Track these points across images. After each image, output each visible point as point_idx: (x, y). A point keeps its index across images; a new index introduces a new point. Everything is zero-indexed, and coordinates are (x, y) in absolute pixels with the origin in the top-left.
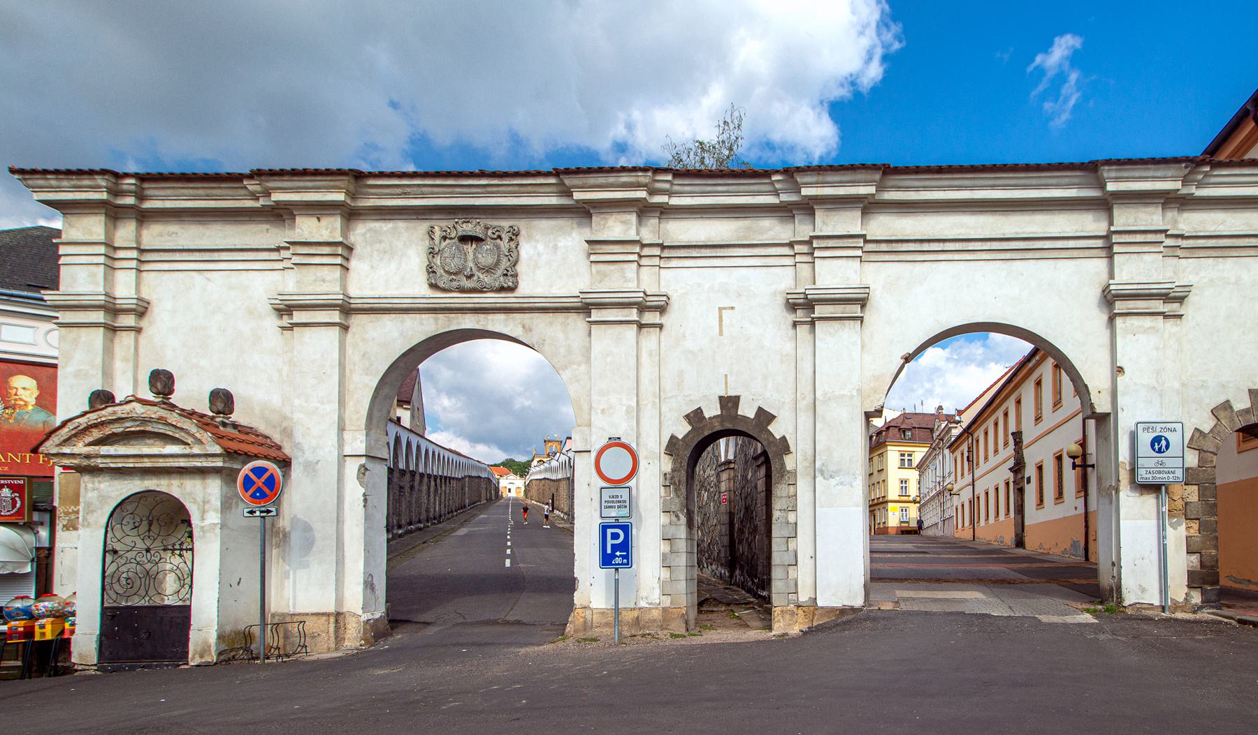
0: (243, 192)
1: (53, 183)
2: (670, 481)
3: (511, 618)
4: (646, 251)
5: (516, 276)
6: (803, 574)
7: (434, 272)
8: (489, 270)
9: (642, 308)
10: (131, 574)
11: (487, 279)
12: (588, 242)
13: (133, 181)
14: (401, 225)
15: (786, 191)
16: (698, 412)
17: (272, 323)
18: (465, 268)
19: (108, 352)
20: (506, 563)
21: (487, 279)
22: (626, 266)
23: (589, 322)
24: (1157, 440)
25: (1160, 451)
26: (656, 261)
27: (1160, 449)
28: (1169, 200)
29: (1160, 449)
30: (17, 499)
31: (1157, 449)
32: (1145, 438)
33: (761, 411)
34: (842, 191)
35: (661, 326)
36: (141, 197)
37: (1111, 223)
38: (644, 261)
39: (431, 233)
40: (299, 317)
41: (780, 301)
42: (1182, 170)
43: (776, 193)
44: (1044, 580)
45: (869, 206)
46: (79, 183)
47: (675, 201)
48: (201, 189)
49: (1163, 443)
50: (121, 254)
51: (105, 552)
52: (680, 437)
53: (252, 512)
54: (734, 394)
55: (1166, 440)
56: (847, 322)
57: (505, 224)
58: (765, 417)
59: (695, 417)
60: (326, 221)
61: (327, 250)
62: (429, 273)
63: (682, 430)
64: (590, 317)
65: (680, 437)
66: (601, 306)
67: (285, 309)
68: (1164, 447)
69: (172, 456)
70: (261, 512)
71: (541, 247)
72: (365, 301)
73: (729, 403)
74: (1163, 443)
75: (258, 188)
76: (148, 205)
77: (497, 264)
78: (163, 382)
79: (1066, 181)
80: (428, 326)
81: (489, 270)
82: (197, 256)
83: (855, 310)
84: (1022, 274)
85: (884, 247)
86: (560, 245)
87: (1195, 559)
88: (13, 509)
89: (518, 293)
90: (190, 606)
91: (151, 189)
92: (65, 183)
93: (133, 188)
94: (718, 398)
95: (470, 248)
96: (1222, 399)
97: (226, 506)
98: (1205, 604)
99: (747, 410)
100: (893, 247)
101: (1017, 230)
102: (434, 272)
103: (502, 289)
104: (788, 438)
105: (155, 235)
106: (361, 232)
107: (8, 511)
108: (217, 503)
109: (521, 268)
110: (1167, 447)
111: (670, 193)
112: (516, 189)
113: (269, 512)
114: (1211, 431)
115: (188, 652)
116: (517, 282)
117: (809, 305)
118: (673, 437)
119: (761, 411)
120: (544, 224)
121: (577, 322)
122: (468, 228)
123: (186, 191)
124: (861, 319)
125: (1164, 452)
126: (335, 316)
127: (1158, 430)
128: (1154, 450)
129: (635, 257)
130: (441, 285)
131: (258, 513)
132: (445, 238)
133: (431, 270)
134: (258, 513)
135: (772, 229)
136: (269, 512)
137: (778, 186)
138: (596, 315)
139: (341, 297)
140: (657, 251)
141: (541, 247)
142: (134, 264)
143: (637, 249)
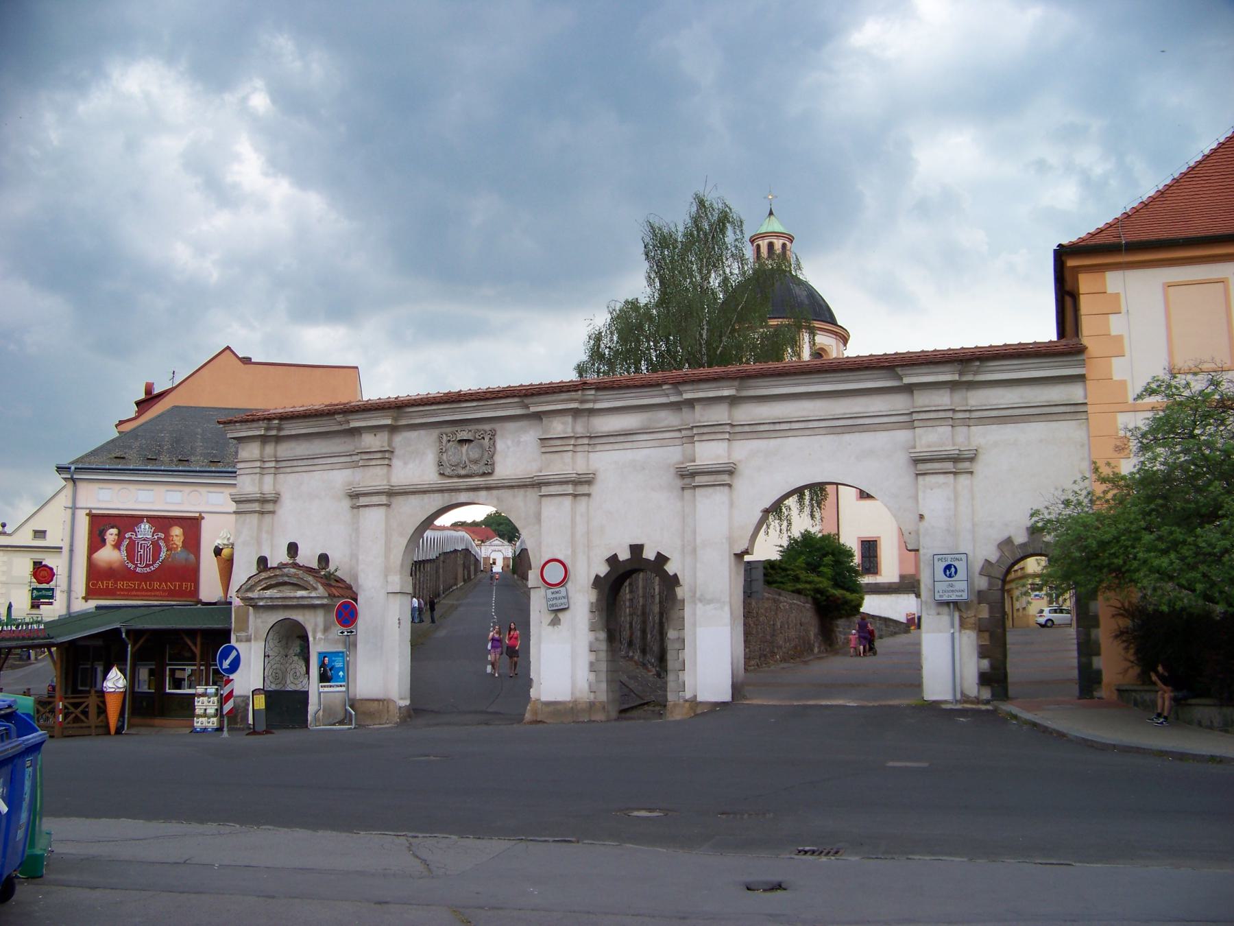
0: (334, 421)
1: (238, 427)
2: (596, 608)
3: (490, 710)
4: (580, 441)
5: (493, 464)
6: (687, 677)
7: (442, 465)
8: (476, 462)
9: (576, 483)
10: (278, 671)
11: (475, 468)
12: (540, 439)
13: (277, 422)
14: (422, 432)
15: (673, 394)
16: (615, 556)
17: (346, 503)
18: (461, 462)
19: (260, 528)
20: (488, 669)
21: (475, 468)
22: (565, 454)
23: (540, 495)
24: (948, 567)
25: (950, 576)
26: (586, 448)
27: (950, 574)
28: (953, 386)
29: (950, 574)
30: (162, 543)
31: (948, 575)
32: (940, 566)
33: (659, 555)
34: (711, 394)
35: (589, 495)
36: (279, 429)
37: (913, 402)
38: (579, 448)
39: (440, 438)
40: (363, 501)
41: (673, 471)
42: (957, 367)
43: (667, 395)
44: (944, 706)
45: (733, 401)
46: (251, 426)
47: (598, 406)
48: (312, 422)
49: (953, 569)
50: (267, 465)
51: (265, 656)
52: (602, 575)
53: (342, 633)
54: (639, 543)
55: (955, 567)
56: (718, 488)
57: (487, 427)
58: (662, 559)
59: (613, 560)
60: (379, 436)
61: (379, 455)
62: (439, 466)
63: (603, 570)
64: (541, 492)
65: (602, 575)
66: (548, 484)
67: (354, 496)
68: (953, 572)
69: (302, 598)
70: (348, 632)
71: (509, 442)
72: (401, 487)
73: (637, 549)
74: (953, 569)
75: (343, 419)
76: (283, 433)
77: (481, 458)
78: (293, 549)
79: (875, 376)
80: (437, 501)
81: (476, 462)
82: (305, 462)
83: (725, 478)
84: (850, 444)
85: (747, 429)
86: (522, 440)
87: (985, 663)
88: (154, 562)
89: (496, 476)
90: (308, 691)
91: (286, 425)
92: (244, 427)
93: (277, 425)
94: (614, 553)
95: (465, 448)
96: (1005, 536)
97: (326, 629)
98: (452, 528)
99: (649, 554)
100: (754, 431)
101: (570, 567)
102: (442, 465)
103: (484, 474)
104: (678, 574)
105: (285, 450)
106: (399, 439)
107: (147, 566)
108: (321, 626)
109: (497, 458)
110: (956, 572)
111: (595, 401)
112: (494, 406)
113: (352, 632)
114: (998, 561)
115: (308, 720)
116: (494, 469)
117: (693, 475)
118: (597, 577)
119: (659, 555)
120: (511, 426)
121: (532, 494)
122: (464, 435)
123: (303, 424)
124: (730, 486)
125: (953, 577)
126: (383, 499)
127: (949, 560)
128: (946, 575)
129: (571, 448)
130: (446, 473)
131: (346, 633)
132: (449, 441)
133: (440, 464)
134: (346, 633)
135: (668, 418)
136: (352, 632)
137: (667, 392)
138: (545, 490)
139: (387, 487)
140: (586, 441)
141: (509, 442)
142: (273, 470)
143: (572, 442)
